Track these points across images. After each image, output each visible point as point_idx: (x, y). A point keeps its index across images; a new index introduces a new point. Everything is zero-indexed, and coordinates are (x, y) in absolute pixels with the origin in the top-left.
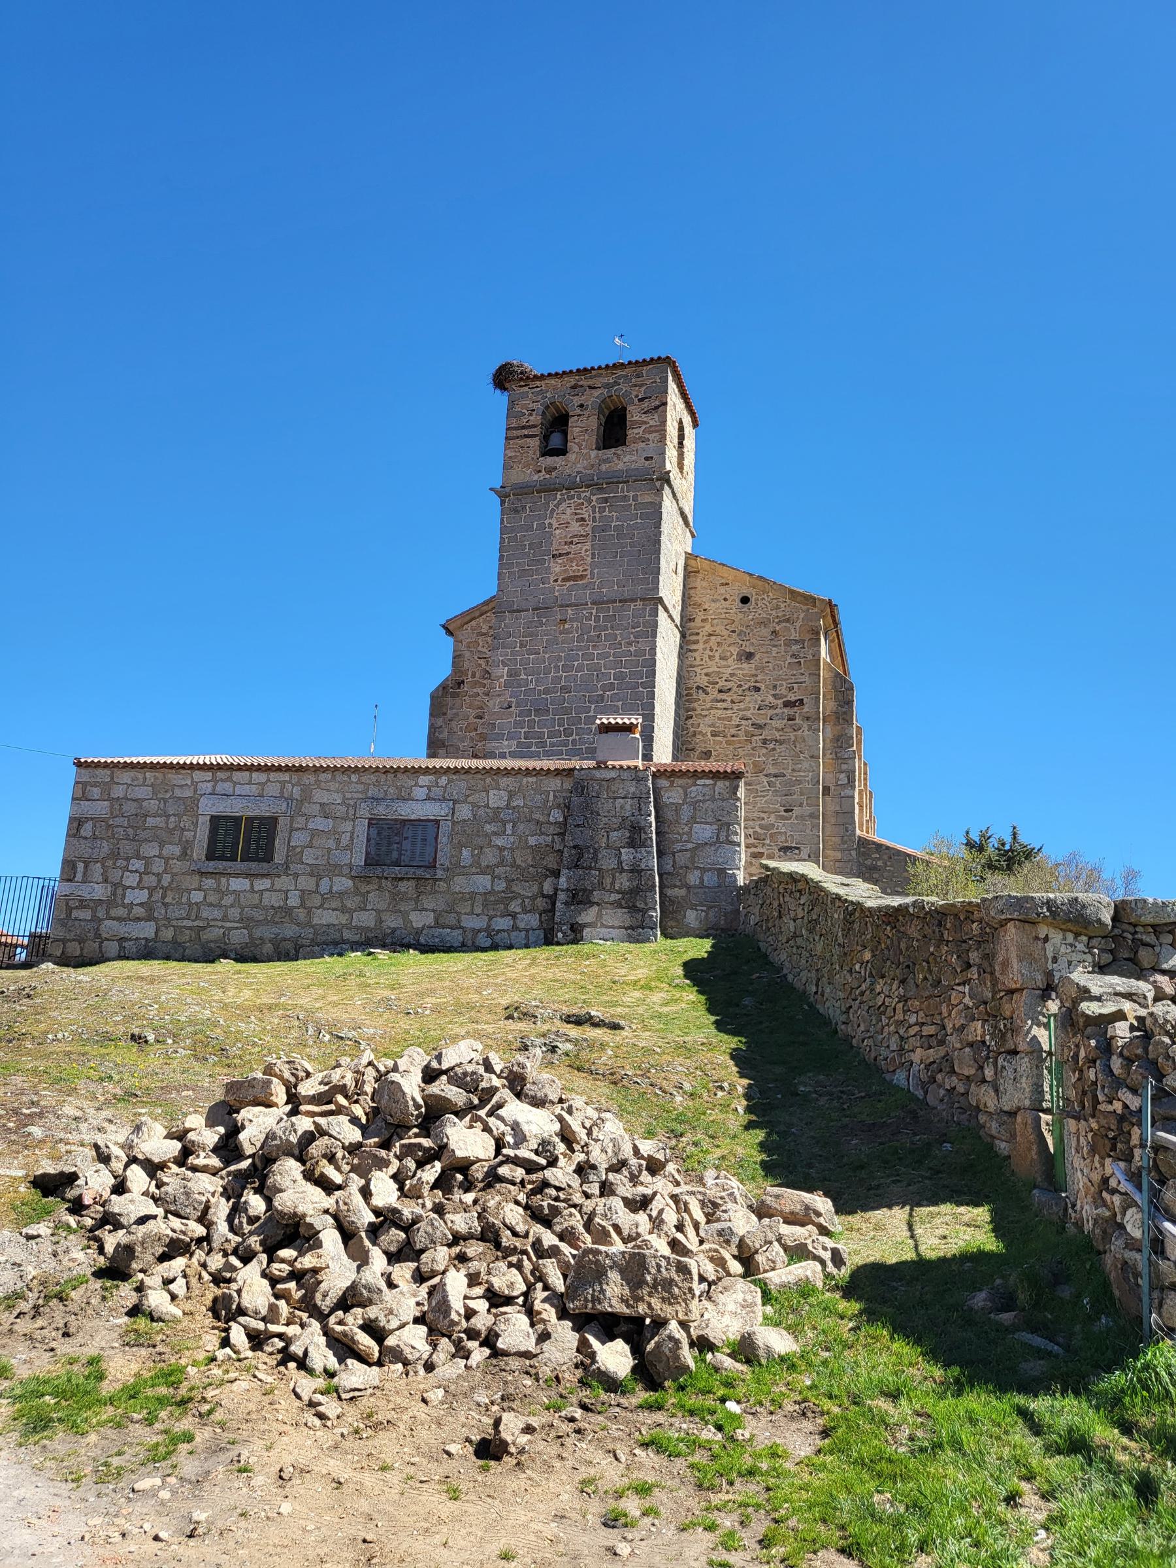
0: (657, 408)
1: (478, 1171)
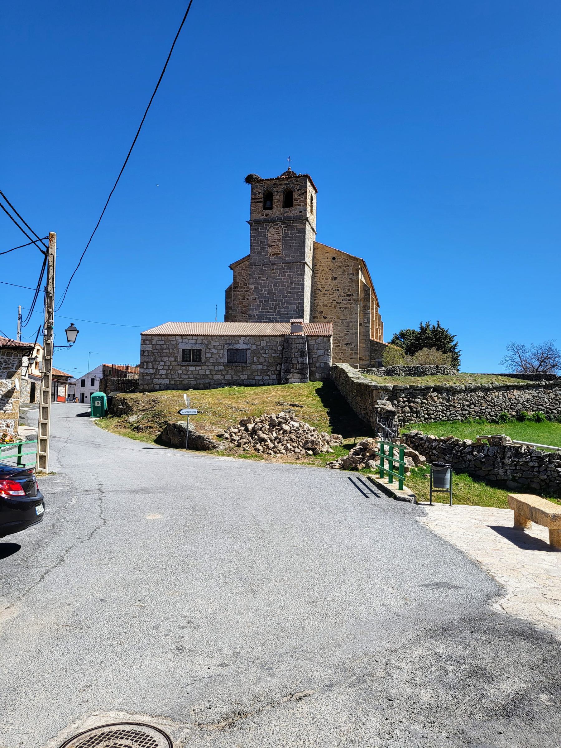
0: (303, 193)
1: (288, 432)
